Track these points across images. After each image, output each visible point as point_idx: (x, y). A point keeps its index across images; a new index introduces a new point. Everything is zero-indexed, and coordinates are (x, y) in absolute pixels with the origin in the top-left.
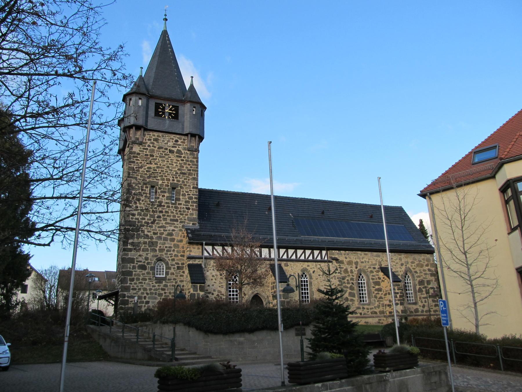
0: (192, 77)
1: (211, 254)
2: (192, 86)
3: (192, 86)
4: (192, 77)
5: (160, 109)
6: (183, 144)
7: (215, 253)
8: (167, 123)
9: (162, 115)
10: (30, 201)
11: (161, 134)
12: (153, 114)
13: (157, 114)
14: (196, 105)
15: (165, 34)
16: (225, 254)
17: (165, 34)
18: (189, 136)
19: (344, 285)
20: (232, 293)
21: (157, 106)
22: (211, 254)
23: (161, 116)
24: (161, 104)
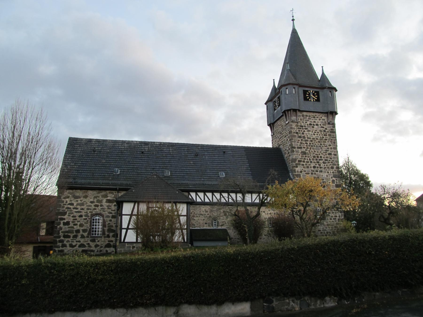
0: (322, 67)
1: (211, 200)
2: (323, 74)
3: (323, 74)
4: (322, 67)
5: (307, 94)
6: (320, 120)
7: (223, 199)
8: (311, 105)
9: (309, 99)
10: (284, 183)
11: (317, 114)
12: (303, 99)
13: (306, 99)
14: (295, 86)
15: (294, 34)
16: (223, 199)
17: (294, 34)
18: (292, 111)
19: (66, 206)
20: (94, 227)
21: (305, 92)
22: (211, 200)
23: (308, 100)
24: (307, 91)
